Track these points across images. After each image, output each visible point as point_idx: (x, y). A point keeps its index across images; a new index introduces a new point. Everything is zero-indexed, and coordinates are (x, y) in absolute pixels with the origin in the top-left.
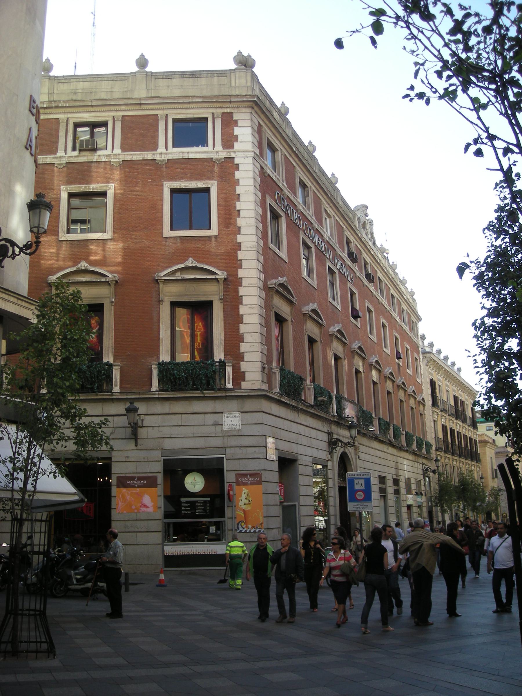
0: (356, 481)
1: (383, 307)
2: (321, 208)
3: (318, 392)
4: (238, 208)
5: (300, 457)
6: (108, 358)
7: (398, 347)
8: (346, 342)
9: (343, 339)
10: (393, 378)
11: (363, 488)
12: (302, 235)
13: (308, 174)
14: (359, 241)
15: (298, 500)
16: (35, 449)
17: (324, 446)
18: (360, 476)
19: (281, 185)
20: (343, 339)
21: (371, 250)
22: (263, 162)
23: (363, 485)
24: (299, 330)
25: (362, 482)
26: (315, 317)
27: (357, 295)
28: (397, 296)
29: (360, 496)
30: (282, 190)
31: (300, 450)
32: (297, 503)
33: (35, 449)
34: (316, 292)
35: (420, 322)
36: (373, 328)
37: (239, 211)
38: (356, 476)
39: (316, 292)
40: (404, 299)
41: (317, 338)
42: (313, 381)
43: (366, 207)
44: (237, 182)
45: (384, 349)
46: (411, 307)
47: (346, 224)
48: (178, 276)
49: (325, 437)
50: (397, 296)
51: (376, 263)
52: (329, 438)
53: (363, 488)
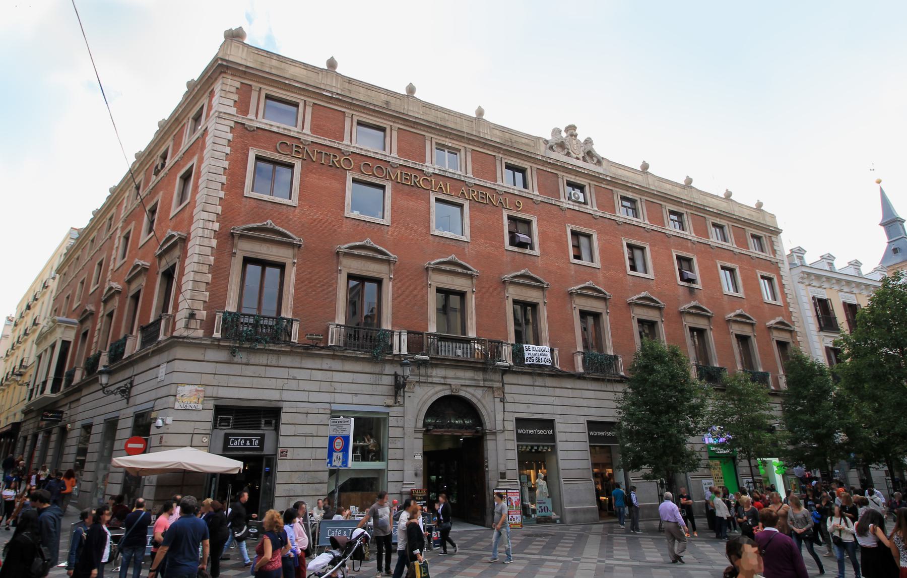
5: (284, 404)
6: (387, 325)
31: (286, 396)
48: (521, 281)
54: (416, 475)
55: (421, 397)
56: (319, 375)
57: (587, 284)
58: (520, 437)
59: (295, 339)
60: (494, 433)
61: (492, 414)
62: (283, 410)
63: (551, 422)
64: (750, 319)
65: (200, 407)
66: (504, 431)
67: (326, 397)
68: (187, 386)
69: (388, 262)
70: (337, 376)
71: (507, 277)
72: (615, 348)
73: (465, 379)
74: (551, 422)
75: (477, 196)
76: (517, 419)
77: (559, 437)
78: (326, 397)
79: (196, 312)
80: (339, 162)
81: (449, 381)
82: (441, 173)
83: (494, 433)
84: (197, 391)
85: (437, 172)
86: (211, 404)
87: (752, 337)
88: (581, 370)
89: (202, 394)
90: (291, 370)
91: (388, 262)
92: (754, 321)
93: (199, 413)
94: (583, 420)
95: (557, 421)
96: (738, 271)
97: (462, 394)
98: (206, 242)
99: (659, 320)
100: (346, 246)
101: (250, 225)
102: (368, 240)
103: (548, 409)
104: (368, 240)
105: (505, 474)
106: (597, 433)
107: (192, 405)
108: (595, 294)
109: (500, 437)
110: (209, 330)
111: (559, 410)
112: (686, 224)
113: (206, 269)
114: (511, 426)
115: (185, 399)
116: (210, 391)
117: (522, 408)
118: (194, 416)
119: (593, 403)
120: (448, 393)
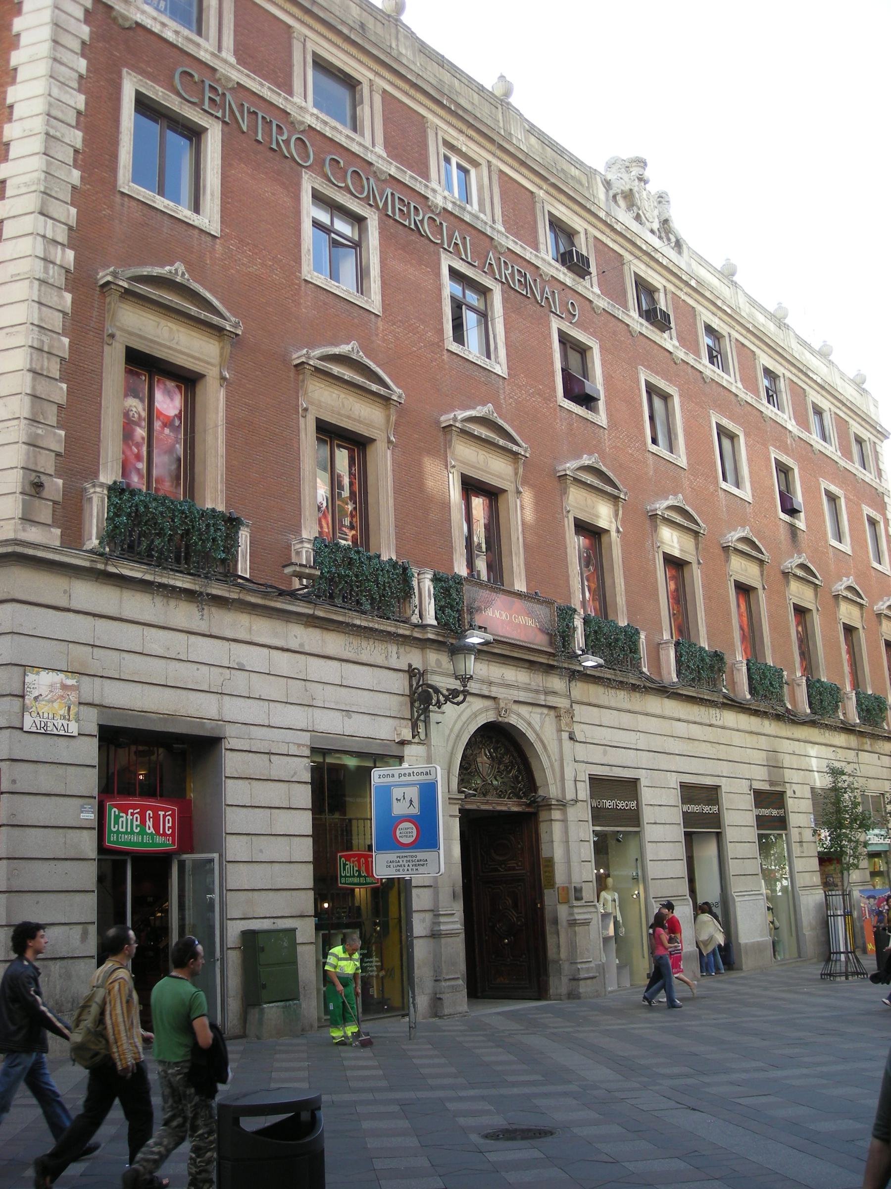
0: (397, 793)
1: (727, 394)
2: (848, 434)
3: (813, 686)
4: (9, 101)
5: (229, 731)
7: (675, 424)
8: (817, 582)
9: (510, 445)
10: (859, 600)
11: (415, 810)
12: (555, 324)
13: (346, 46)
14: (607, 231)
15: (219, 848)
16: (474, 795)
17: (396, 705)
18: (407, 778)
19: (734, 390)
20: (510, 445)
21: (658, 256)
22: (426, 186)
23: (416, 803)
24: (831, 616)
25: (413, 793)
26: (501, 442)
27: (796, 471)
28: (788, 374)
29: (406, 833)
30: (214, 70)
31: (234, 709)
32: (216, 856)
33: (474, 795)
34: (380, 324)
35: (886, 441)
36: (676, 435)
37: (11, 107)
38: (396, 778)
39: (380, 324)
40: (815, 382)
41: (857, 624)
42: (856, 685)
43: (642, 163)
44: (14, 42)
45: (723, 485)
46: (844, 404)
47: (545, 187)
49: (400, 683)
50: (788, 374)
51: (686, 289)
52: (411, 686)
53: (415, 810)
54: (454, 896)
55: (456, 723)
56: (283, 663)
57: (343, 349)
58: (598, 815)
59: (243, 568)
60: (563, 805)
61: (557, 765)
62: (225, 744)
63: (634, 783)
64: (615, 486)
65: (73, 729)
66: (576, 801)
67: (297, 717)
68: (43, 673)
69: (386, 400)
70: (318, 669)
71: (733, 537)
72: (631, 614)
73: (518, 688)
74: (634, 783)
75: (512, 275)
76: (684, 786)
77: (648, 815)
78: (297, 717)
79: (44, 478)
80: (287, 142)
81: (495, 691)
82: (457, 212)
83: (563, 805)
84: (64, 687)
85: (450, 207)
86: (91, 722)
87: (695, 566)
88: (671, 675)
89: (73, 697)
90: (234, 645)
91: (386, 400)
92: (766, 557)
93: (72, 742)
94: (674, 781)
95: (643, 782)
96: (676, 400)
97: (513, 720)
98: (53, 298)
99: (212, 374)
100: (318, 352)
101: (146, 271)
102: (180, 266)
103: (627, 758)
104: (180, 266)
105: (581, 890)
106: (706, 809)
107: (59, 722)
108: (359, 379)
109: (573, 813)
110: (73, 535)
111: (645, 759)
112: (364, 112)
113: (54, 369)
114: (584, 792)
115: (44, 708)
116: (91, 689)
117: (596, 754)
118: (62, 751)
119: (133, 665)
120: (491, 717)
